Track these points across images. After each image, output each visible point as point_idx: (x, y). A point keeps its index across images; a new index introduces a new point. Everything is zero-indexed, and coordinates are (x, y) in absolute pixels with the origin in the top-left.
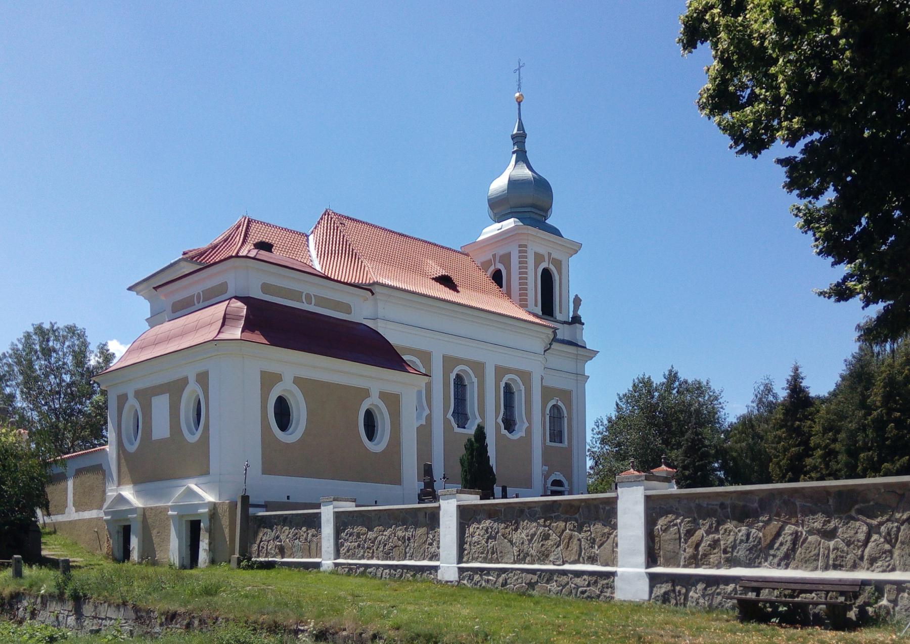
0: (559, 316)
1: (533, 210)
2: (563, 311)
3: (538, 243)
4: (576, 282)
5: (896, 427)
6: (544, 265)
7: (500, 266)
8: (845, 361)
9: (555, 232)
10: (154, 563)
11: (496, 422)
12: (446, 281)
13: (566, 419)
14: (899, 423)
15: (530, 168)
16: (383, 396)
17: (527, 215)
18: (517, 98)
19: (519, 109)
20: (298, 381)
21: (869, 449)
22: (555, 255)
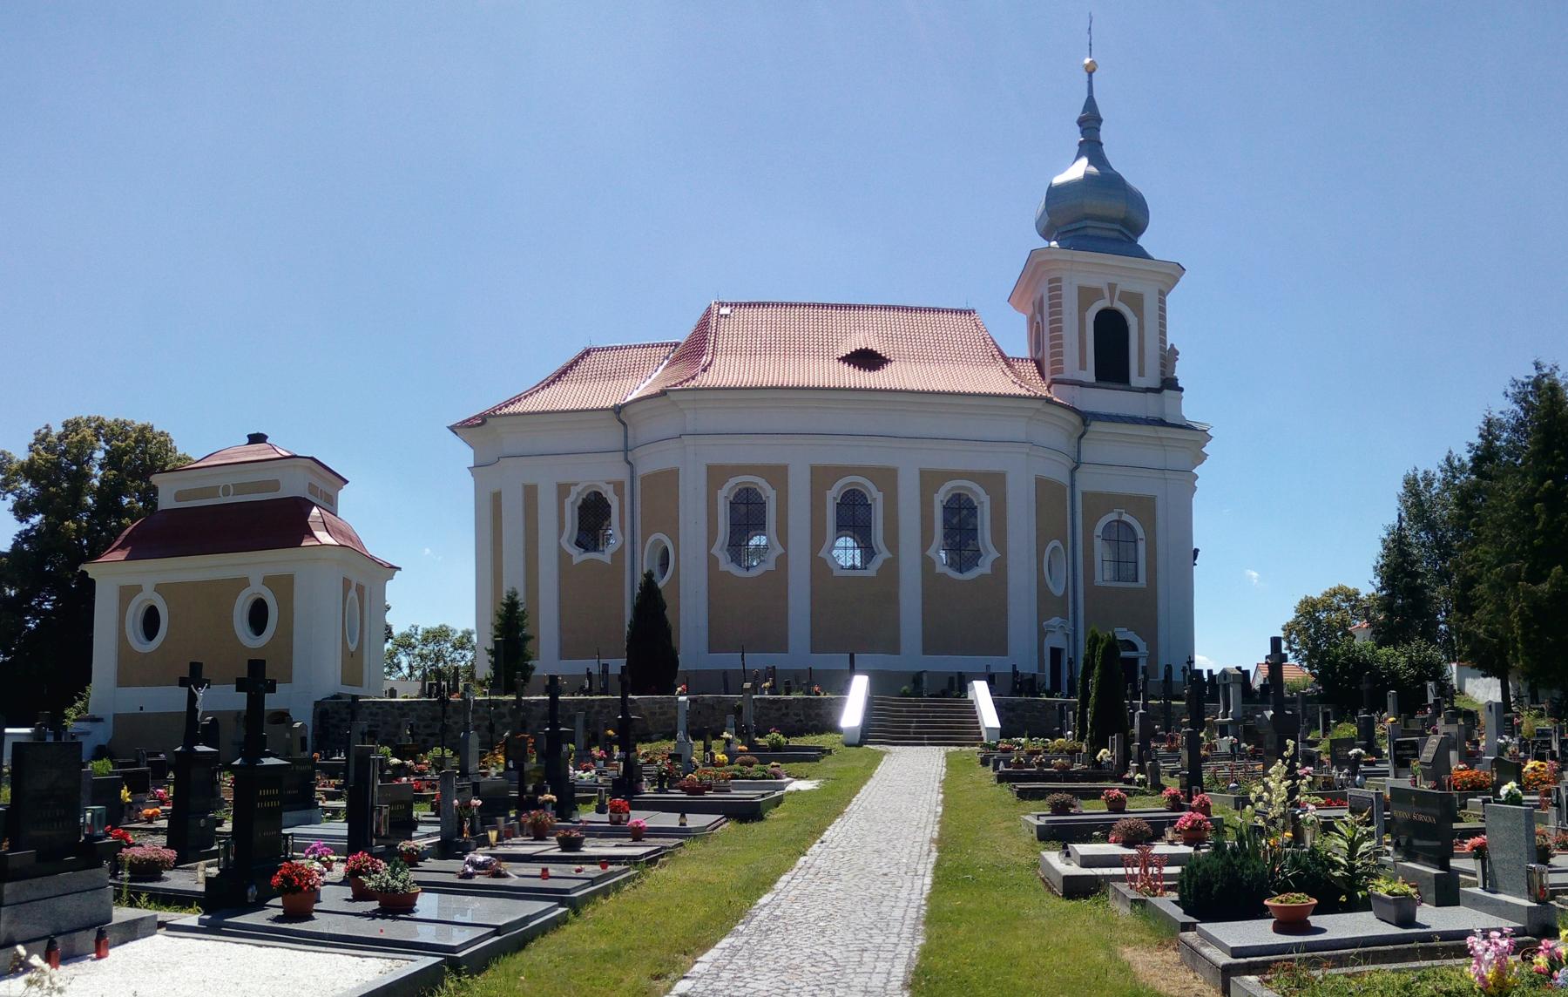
0: (1135, 380)
1: (1089, 223)
2: (1143, 372)
3: (1097, 271)
9: (1142, 254)
13: (1142, 546)
16: (269, 581)
17: (1081, 233)
18: (1087, 67)
20: (159, 588)
21: (1519, 556)
22: (1125, 285)
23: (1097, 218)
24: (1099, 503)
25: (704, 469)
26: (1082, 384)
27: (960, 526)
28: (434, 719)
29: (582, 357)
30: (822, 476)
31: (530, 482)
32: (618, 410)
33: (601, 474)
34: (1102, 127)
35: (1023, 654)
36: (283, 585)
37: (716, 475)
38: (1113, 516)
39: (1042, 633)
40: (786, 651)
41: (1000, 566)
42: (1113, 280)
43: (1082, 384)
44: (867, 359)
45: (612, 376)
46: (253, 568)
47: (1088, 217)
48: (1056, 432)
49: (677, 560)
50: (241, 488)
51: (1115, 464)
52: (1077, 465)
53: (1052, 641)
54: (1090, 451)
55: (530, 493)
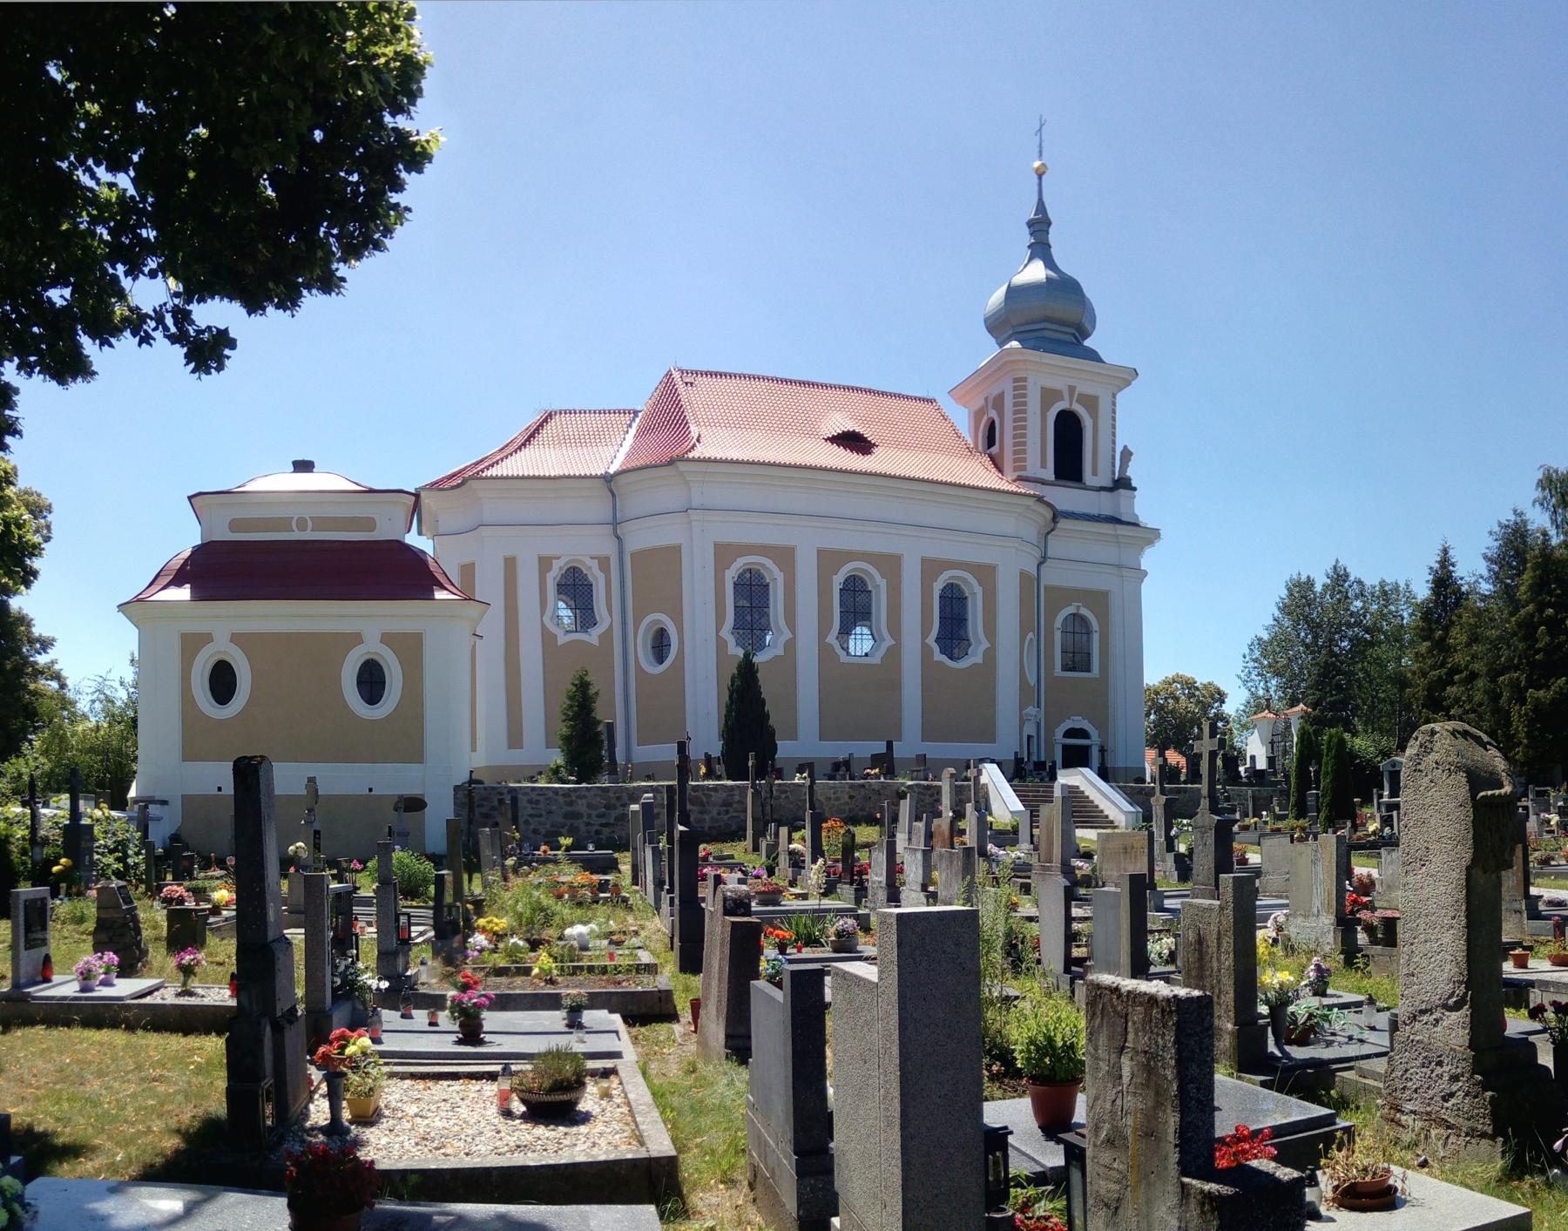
0: (1089, 478)
1: (1050, 326)
3: (1051, 372)
4: (1135, 428)
5: (1550, 632)
6: (1062, 405)
7: (993, 414)
8: (1490, 533)
9: (1093, 356)
10: (1015, 830)
11: (924, 645)
12: (853, 441)
13: (1096, 637)
14: (1554, 626)
15: (1050, 264)
17: (1039, 334)
18: (1037, 170)
19: (1040, 185)
20: (236, 639)
21: (1516, 668)
22: (1083, 388)
23: (1050, 319)
24: (1060, 596)
25: (711, 550)
26: (1043, 482)
27: (752, 598)
28: (608, 807)
29: (546, 421)
30: (828, 560)
31: (509, 554)
32: (607, 479)
33: (585, 547)
34: (1051, 230)
35: (1008, 742)
36: (410, 646)
37: (724, 553)
38: (1071, 610)
39: (1022, 722)
40: (993, 741)
41: (990, 656)
42: (1072, 382)
43: (1043, 482)
44: (853, 441)
45: (580, 441)
46: (368, 623)
47: (1047, 319)
48: (1029, 526)
49: (681, 642)
50: (321, 523)
51: (1078, 558)
52: (1044, 559)
53: (1030, 729)
54: (1056, 546)
55: (510, 564)
